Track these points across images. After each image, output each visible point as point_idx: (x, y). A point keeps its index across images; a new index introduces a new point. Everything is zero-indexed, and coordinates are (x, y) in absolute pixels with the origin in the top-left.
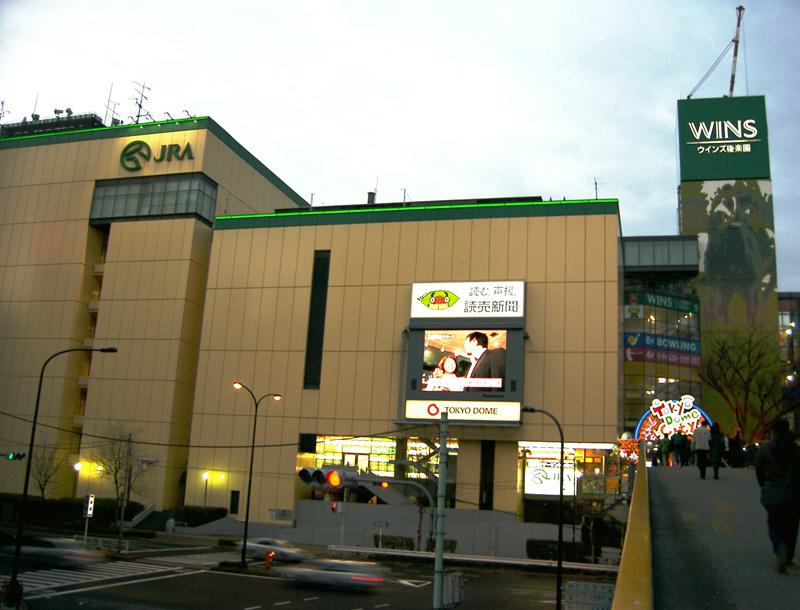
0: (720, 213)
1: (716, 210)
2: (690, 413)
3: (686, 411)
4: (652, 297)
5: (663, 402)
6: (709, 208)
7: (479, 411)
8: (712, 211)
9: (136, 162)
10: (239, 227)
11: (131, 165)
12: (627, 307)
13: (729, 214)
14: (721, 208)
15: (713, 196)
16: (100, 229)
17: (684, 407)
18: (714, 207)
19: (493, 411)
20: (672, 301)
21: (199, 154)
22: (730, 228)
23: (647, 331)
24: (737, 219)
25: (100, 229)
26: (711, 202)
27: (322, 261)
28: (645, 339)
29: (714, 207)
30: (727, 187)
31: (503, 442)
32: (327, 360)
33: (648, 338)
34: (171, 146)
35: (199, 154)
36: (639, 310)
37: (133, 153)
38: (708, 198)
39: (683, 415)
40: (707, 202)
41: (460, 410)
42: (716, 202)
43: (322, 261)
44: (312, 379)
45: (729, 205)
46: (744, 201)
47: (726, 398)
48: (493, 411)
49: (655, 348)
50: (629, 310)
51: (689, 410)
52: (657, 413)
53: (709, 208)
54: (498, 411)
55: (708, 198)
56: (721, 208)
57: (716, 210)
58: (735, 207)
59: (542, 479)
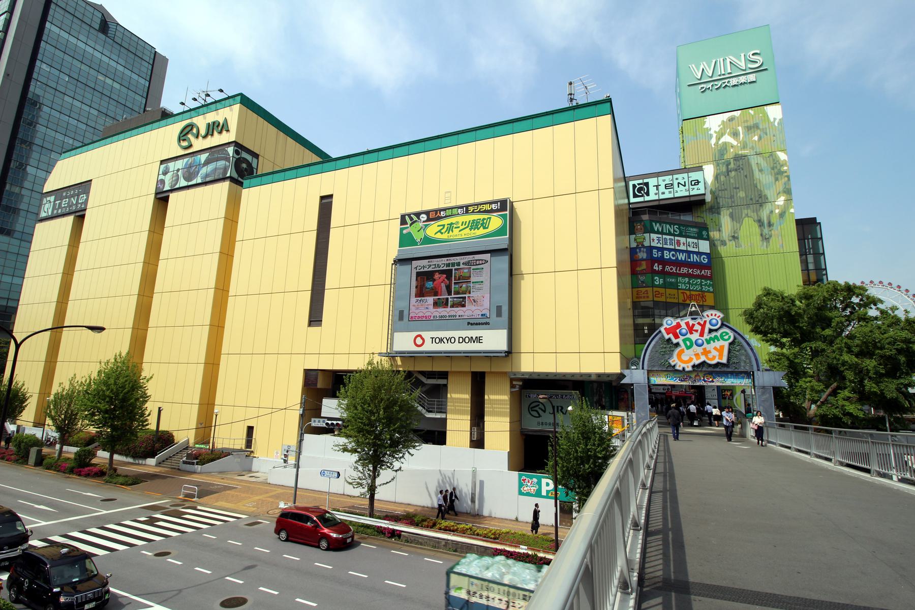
0: (725, 144)
1: (722, 140)
2: (718, 334)
3: (711, 331)
4: (658, 225)
5: (679, 320)
6: (713, 141)
7: (464, 340)
8: (717, 144)
9: (189, 140)
10: (448, 254)
11: (185, 144)
12: (633, 237)
13: (735, 143)
14: (727, 138)
15: (718, 129)
16: (162, 200)
17: (708, 326)
18: (718, 139)
19: (478, 340)
20: (679, 228)
21: (233, 125)
22: (737, 158)
23: (653, 244)
24: (744, 147)
25: (162, 200)
26: (715, 135)
27: (326, 203)
28: (652, 253)
29: (718, 139)
30: (731, 119)
31: (491, 373)
32: (329, 297)
33: (655, 251)
34: (214, 123)
35: (233, 125)
36: (644, 239)
37: (187, 133)
38: (712, 132)
39: (706, 336)
40: (711, 136)
41: (445, 340)
42: (720, 135)
43: (326, 203)
44: (315, 318)
45: (735, 134)
46: (751, 128)
47: (27, 404)
48: (478, 340)
49: (662, 261)
50: (635, 240)
51: (716, 330)
52: (671, 336)
53: (713, 141)
54: (484, 340)
55: (712, 132)
56: (727, 138)
57: (722, 140)
58: (741, 136)
59: (540, 412)
